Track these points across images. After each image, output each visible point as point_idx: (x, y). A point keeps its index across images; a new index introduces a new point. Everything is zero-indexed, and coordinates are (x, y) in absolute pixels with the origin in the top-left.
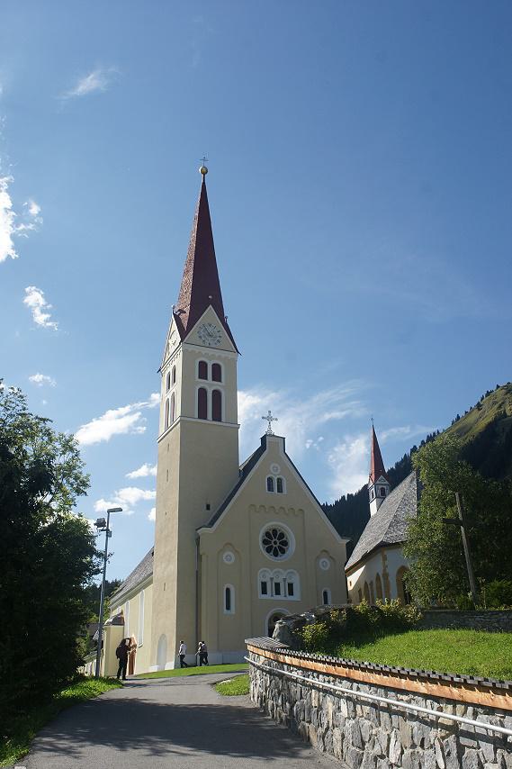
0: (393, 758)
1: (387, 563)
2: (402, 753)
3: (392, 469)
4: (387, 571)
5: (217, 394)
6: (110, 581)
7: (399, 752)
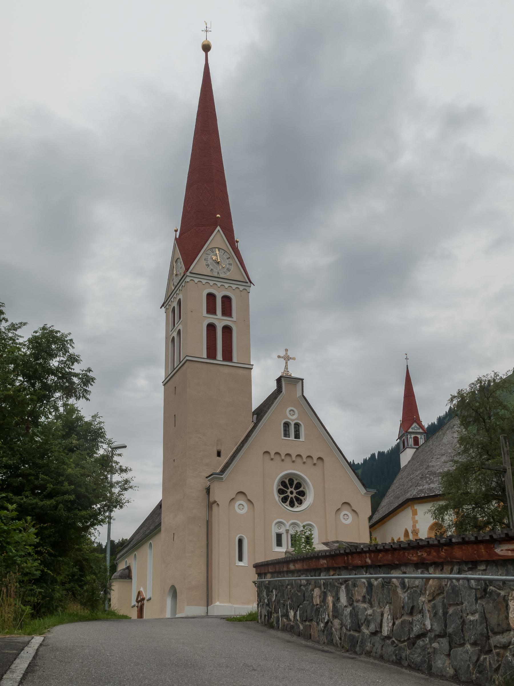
0: (385, 631)
1: (417, 518)
2: (394, 624)
3: (433, 425)
4: (418, 526)
5: (227, 330)
6: (117, 541)
7: (391, 624)
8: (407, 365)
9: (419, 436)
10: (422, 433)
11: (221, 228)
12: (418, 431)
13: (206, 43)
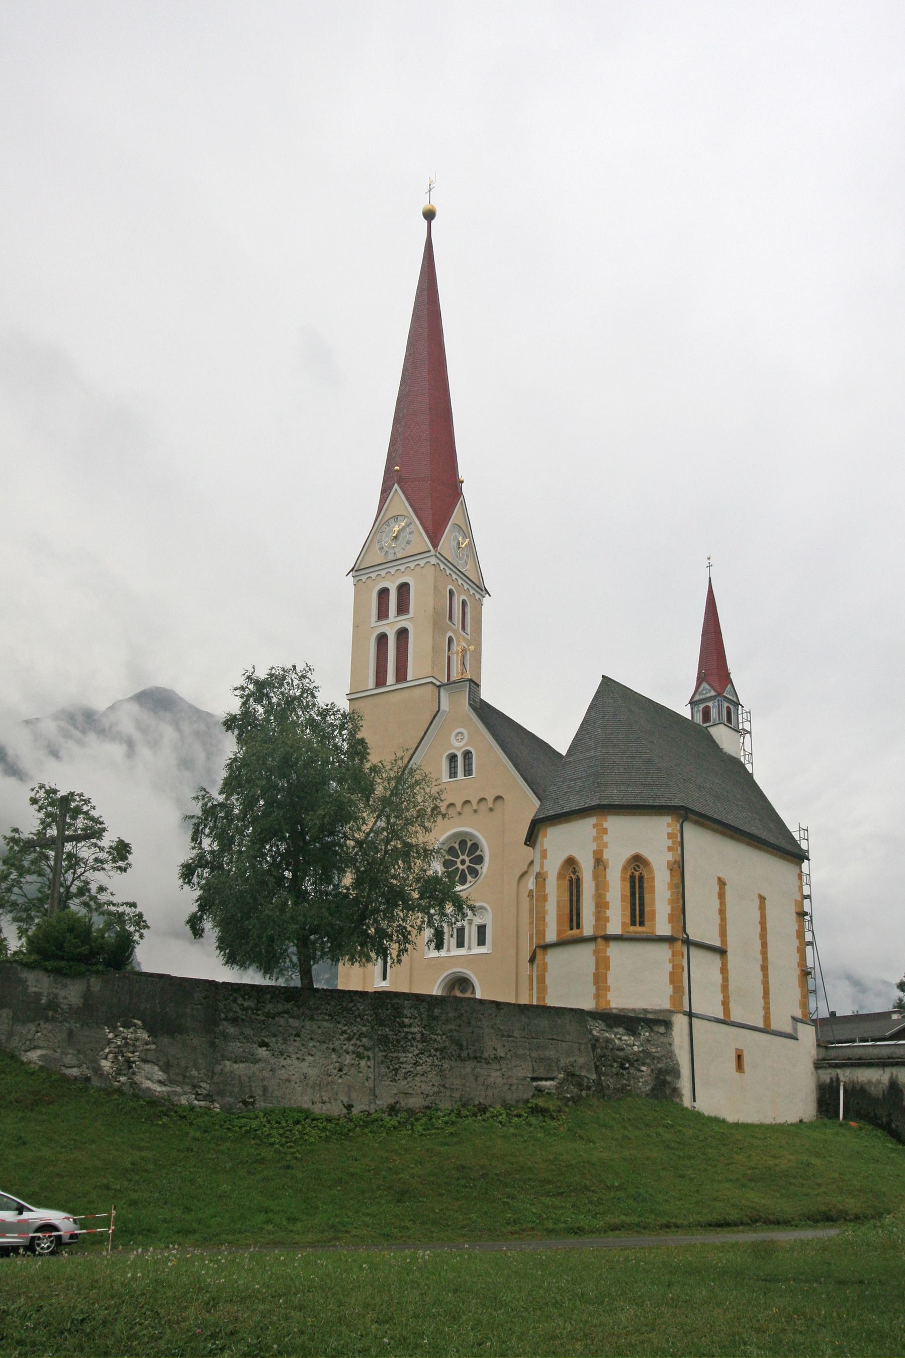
8: (710, 578)
9: (710, 704)
10: (714, 696)
11: (401, 488)
12: (708, 695)
13: (430, 207)
